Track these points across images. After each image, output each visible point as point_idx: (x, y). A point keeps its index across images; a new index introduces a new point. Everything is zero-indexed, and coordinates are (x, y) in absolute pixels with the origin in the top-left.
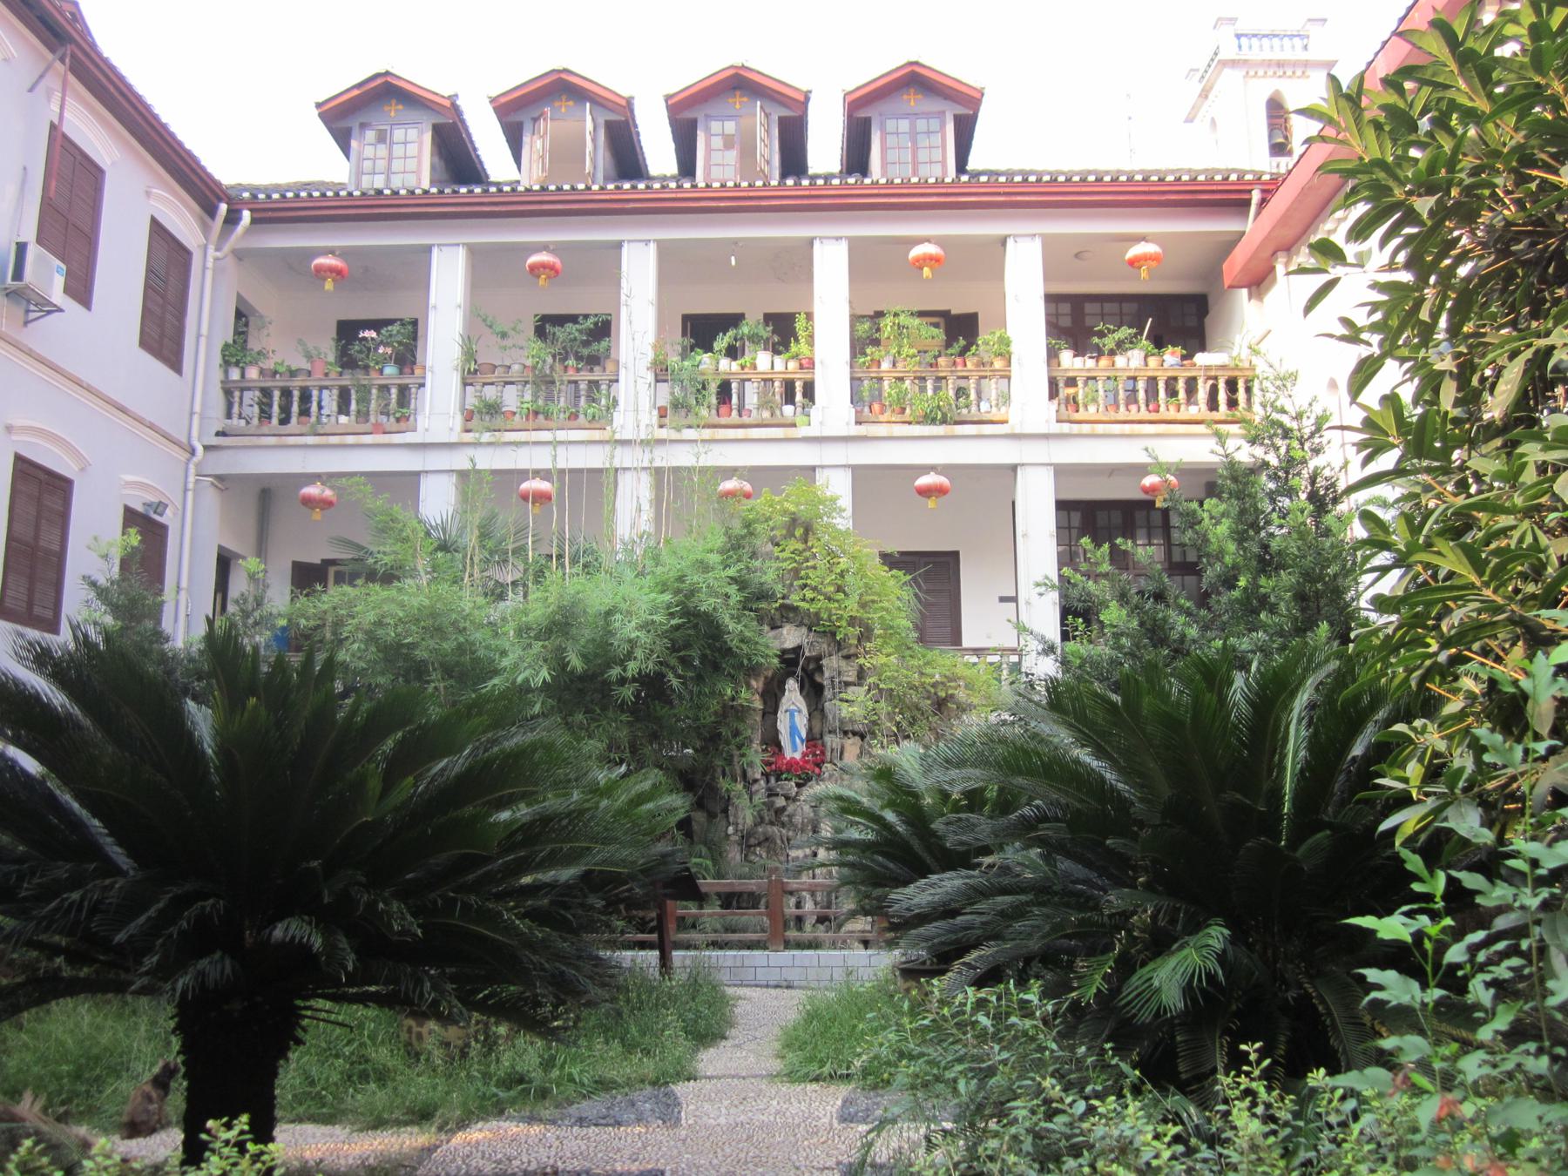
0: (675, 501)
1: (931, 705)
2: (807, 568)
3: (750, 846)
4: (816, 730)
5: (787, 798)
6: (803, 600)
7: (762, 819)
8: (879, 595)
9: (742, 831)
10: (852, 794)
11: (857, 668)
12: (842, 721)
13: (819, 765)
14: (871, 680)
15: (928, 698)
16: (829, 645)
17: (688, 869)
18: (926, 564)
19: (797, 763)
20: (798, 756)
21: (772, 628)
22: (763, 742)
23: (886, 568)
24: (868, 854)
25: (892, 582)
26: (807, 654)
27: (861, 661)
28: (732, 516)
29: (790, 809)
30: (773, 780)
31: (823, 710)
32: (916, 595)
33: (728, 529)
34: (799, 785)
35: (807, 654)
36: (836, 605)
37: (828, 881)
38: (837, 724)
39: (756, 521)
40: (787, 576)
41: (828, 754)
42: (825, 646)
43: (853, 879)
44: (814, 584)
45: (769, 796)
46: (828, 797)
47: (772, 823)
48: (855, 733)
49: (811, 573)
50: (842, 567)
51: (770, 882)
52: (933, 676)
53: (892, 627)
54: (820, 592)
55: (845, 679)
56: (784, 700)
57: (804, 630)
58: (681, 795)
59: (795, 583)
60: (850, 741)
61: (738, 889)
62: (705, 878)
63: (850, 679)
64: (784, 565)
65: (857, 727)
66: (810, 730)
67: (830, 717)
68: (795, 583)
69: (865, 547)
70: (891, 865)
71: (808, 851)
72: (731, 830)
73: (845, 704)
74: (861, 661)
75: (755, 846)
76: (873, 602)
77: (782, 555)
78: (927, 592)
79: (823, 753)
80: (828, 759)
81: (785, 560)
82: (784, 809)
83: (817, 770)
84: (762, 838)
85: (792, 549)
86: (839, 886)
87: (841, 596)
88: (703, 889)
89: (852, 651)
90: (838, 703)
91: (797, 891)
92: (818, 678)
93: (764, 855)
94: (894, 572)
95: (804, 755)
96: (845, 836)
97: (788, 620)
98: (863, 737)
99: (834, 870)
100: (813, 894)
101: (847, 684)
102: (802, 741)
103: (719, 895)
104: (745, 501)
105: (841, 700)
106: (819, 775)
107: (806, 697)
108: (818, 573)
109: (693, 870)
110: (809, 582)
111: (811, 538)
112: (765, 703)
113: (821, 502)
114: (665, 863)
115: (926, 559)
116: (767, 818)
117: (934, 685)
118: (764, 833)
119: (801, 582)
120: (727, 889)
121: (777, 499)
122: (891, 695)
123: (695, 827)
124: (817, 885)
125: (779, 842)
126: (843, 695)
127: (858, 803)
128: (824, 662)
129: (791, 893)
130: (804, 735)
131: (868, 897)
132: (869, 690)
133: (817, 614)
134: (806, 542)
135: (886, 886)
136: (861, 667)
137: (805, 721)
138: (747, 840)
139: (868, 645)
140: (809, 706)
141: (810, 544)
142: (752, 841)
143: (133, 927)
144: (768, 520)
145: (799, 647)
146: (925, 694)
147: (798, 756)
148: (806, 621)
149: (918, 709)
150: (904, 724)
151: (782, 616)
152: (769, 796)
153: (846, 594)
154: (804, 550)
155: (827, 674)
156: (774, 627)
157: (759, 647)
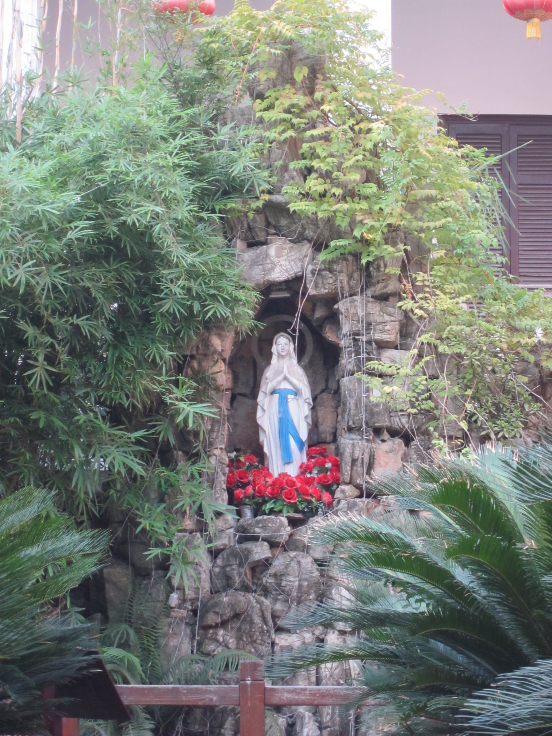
0: (82, 17)
1: (531, 383)
2: (313, 138)
3: (206, 628)
4: (326, 427)
5: (273, 545)
6: (306, 196)
7: (228, 578)
8: (440, 188)
9: (194, 601)
10: (395, 532)
11: (399, 316)
12: (371, 411)
13: (329, 488)
14: (425, 338)
15: (524, 372)
16: (350, 277)
17: (99, 664)
18: (521, 138)
19: (291, 483)
20: (293, 471)
21: (251, 245)
22: (232, 447)
23: (455, 143)
24: (418, 638)
25: (464, 168)
26: (311, 291)
27: (408, 304)
28: (180, 45)
29: (278, 564)
30: (248, 512)
31: (337, 392)
32: (501, 192)
33: (173, 67)
34: (294, 523)
35: (311, 291)
36: (364, 205)
37: (342, 689)
38: (363, 416)
39: (224, 53)
40: (276, 153)
41: (346, 469)
42: (343, 277)
43: (393, 681)
44: (324, 167)
45: (241, 540)
46: (355, 536)
47: (246, 588)
48: (394, 433)
49: (321, 149)
50: (375, 136)
51: (243, 689)
52: (531, 332)
53: (460, 243)
54: (335, 183)
55: (379, 336)
56: (269, 373)
57: (307, 248)
58: (89, 533)
59: (292, 165)
60: (384, 447)
61: (186, 700)
62: (126, 682)
63: (384, 337)
64: (272, 134)
65: (402, 422)
66: (314, 427)
67: (351, 403)
68: (292, 165)
69: (416, 102)
70: (460, 658)
71: (308, 637)
72: (174, 599)
73: (377, 381)
74: (408, 304)
75: (216, 626)
76: (430, 199)
77: (268, 116)
78: (522, 187)
79: (337, 466)
80: (347, 479)
81: (274, 124)
82: (266, 563)
83: (326, 497)
84: (228, 613)
85: (287, 103)
86: (367, 695)
87: (371, 188)
88: (126, 700)
89: (392, 287)
90: (365, 378)
91: (290, 704)
92: (330, 336)
93: (232, 642)
94: (468, 149)
95: (305, 469)
96: (379, 607)
97: (279, 233)
98: (407, 439)
99: (354, 665)
100: (316, 712)
101: (382, 345)
102: (301, 444)
103: (149, 710)
104: (203, 18)
105: (371, 373)
106: (330, 505)
107: (309, 369)
108: (334, 148)
109: (109, 667)
110: (316, 164)
111: (320, 84)
112: (236, 378)
113: (339, 22)
114: (61, 653)
115: (523, 130)
116: (237, 580)
117: (535, 349)
118: (231, 605)
119: (302, 164)
120: (168, 701)
121: (261, 14)
122: (458, 367)
123: (111, 593)
124: (323, 695)
125: (257, 620)
126: (373, 364)
127: (407, 546)
128: (341, 306)
129: (278, 709)
130: (304, 436)
131: (419, 710)
132: (420, 356)
133: (330, 221)
134: (311, 92)
135: (451, 693)
136: (407, 315)
137: (306, 410)
138: (202, 617)
139: (420, 276)
140: (313, 384)
141: (318, 95)
142: (212, 619)
143: (539, 455)
144: (245, 50)
145: (298, 279)
146: (520, 366)
147: (293, 471)
148: (309, 233)
149: (506, 391)
150: (481, 417)
151: (268, 224)
152: (241, 540)
153: (381, 185)
154: (309, 107)
155: (346, 328)
156: (252, 244)
157: (224, 283)
